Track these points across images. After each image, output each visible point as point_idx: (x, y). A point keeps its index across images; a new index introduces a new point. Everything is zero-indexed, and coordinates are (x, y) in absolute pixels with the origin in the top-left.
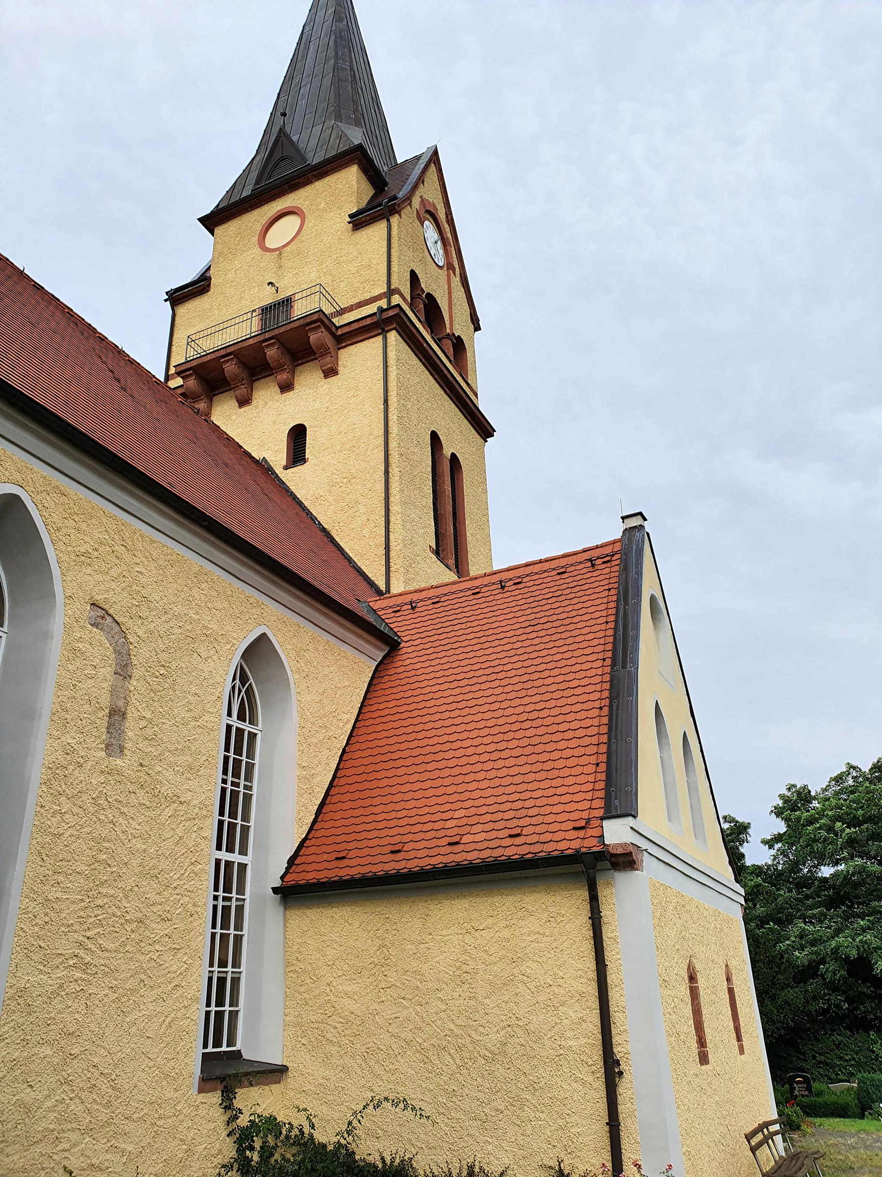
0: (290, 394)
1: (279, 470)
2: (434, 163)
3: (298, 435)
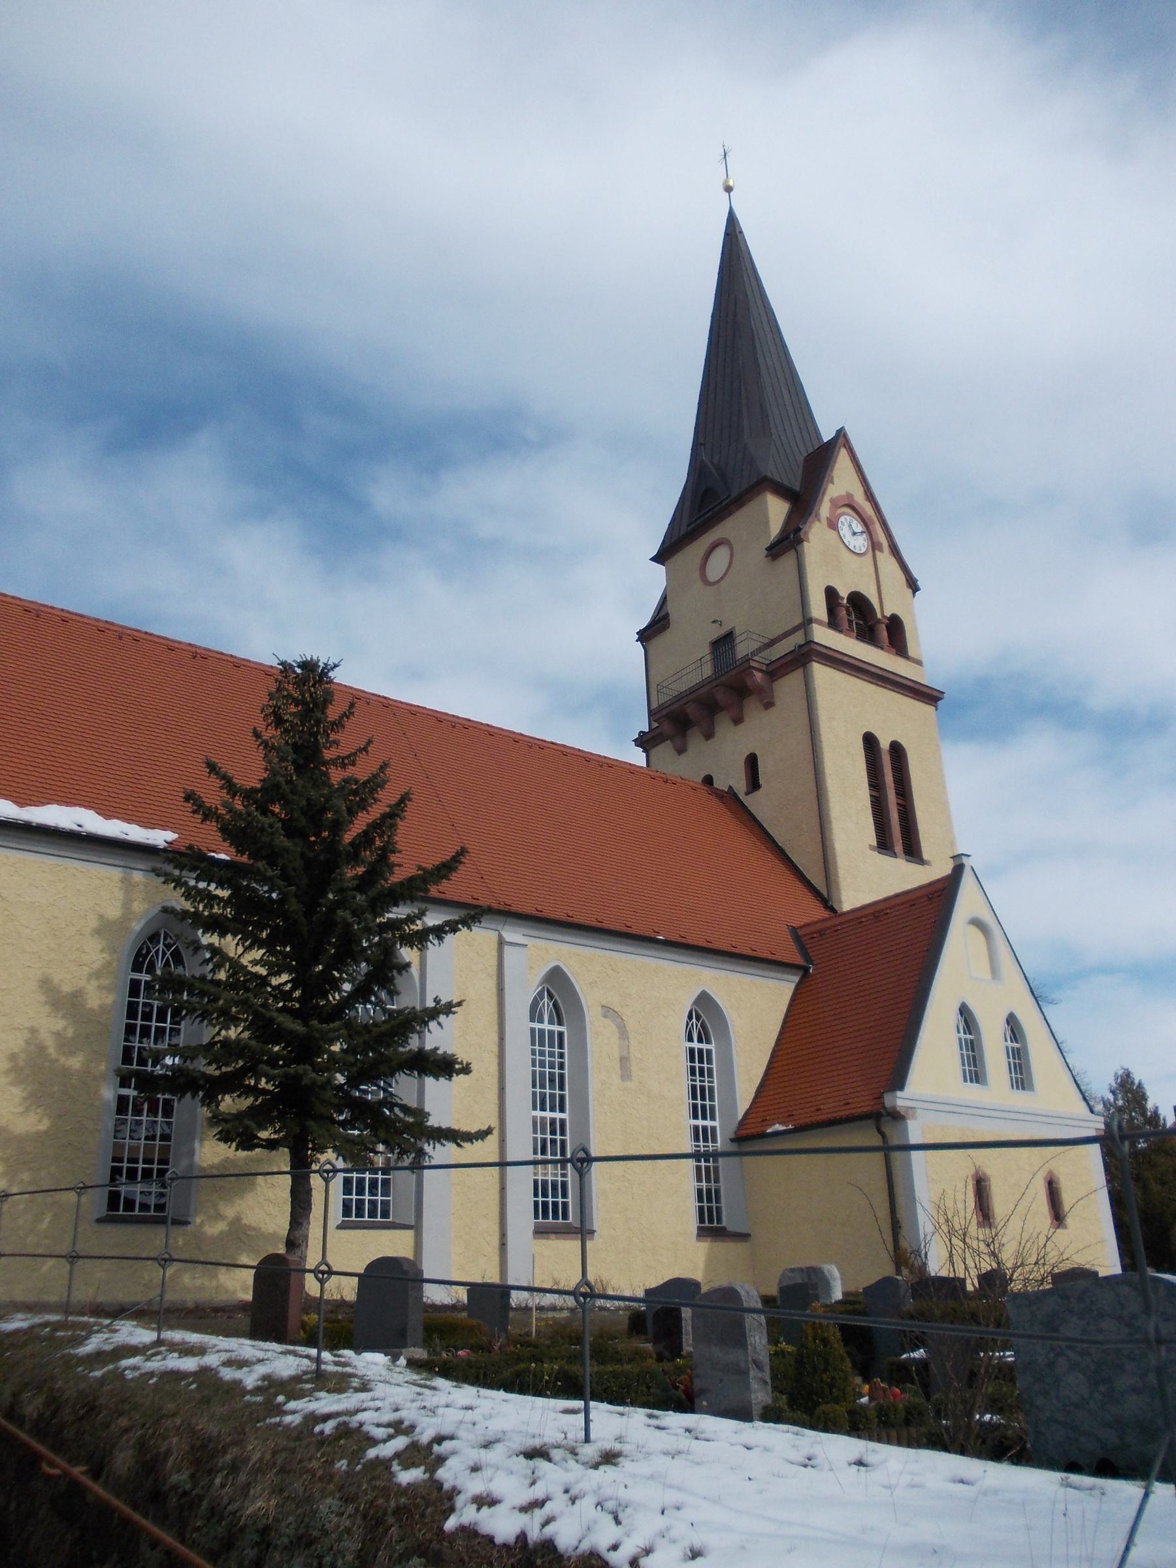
0: (742, 726)
1: (742, 796)
2: (844, 446)
3: (752, 762)
